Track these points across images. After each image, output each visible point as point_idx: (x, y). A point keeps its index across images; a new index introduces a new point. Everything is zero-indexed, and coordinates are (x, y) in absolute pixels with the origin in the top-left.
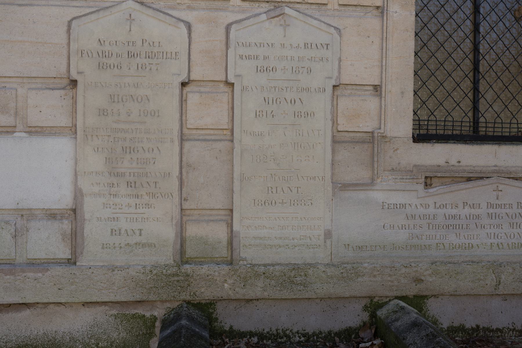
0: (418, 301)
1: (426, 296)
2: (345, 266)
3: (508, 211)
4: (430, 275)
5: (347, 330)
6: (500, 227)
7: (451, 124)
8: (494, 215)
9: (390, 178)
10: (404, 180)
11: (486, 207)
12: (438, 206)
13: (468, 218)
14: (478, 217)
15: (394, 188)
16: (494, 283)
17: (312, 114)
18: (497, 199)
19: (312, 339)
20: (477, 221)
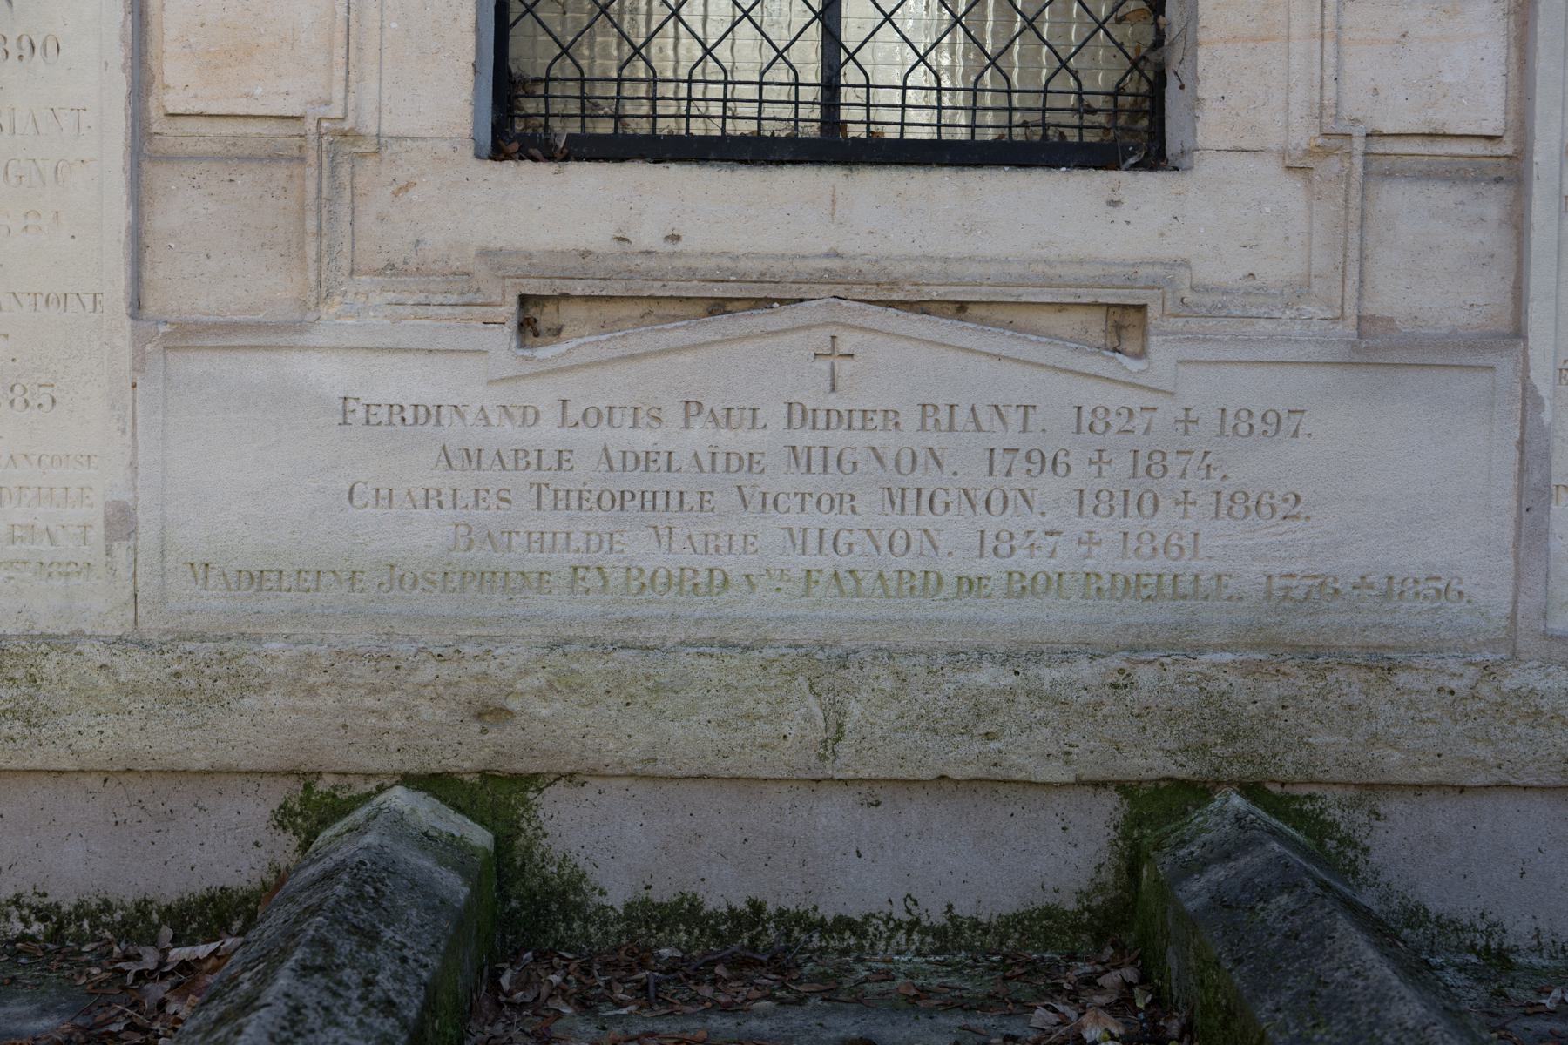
0: (497, 795)
1: (536, 776)
2: (189, 646)
3: (878, 439)
4: (540, 693)
5: (212, 898)
6: (847, 507)
7: (716, 91)
8: (817, 455)
9: (377, 299)
10: (431, 310)
11: (784, 423)
12: (574, 413)
13: (707, 465)
14: (750, 461)
15: (388, 342)
16: (816, 734)
17: (51, 48)
19: (73, 929)
20: (742, 478)
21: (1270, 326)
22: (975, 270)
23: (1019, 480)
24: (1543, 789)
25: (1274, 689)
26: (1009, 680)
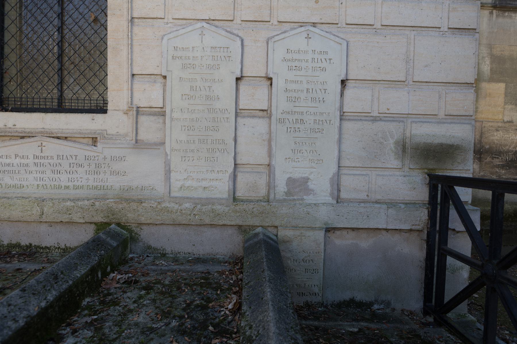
3: (50, 161)
8: (39, 164)
14: (27, 165)
18: (42, 152)
20: (26, 168)
21: (119, 141)
22: (68, 131)
23: (75, 168)
24: (171, 224)
25: (120, 206)
26: (73, 204)
